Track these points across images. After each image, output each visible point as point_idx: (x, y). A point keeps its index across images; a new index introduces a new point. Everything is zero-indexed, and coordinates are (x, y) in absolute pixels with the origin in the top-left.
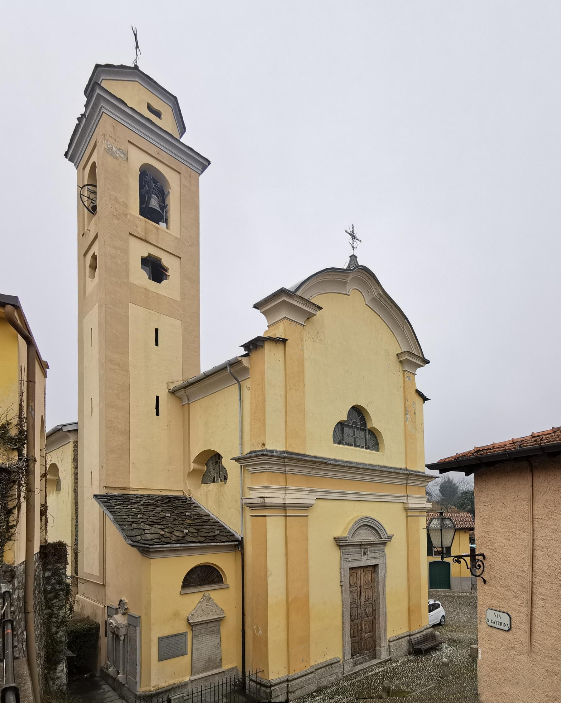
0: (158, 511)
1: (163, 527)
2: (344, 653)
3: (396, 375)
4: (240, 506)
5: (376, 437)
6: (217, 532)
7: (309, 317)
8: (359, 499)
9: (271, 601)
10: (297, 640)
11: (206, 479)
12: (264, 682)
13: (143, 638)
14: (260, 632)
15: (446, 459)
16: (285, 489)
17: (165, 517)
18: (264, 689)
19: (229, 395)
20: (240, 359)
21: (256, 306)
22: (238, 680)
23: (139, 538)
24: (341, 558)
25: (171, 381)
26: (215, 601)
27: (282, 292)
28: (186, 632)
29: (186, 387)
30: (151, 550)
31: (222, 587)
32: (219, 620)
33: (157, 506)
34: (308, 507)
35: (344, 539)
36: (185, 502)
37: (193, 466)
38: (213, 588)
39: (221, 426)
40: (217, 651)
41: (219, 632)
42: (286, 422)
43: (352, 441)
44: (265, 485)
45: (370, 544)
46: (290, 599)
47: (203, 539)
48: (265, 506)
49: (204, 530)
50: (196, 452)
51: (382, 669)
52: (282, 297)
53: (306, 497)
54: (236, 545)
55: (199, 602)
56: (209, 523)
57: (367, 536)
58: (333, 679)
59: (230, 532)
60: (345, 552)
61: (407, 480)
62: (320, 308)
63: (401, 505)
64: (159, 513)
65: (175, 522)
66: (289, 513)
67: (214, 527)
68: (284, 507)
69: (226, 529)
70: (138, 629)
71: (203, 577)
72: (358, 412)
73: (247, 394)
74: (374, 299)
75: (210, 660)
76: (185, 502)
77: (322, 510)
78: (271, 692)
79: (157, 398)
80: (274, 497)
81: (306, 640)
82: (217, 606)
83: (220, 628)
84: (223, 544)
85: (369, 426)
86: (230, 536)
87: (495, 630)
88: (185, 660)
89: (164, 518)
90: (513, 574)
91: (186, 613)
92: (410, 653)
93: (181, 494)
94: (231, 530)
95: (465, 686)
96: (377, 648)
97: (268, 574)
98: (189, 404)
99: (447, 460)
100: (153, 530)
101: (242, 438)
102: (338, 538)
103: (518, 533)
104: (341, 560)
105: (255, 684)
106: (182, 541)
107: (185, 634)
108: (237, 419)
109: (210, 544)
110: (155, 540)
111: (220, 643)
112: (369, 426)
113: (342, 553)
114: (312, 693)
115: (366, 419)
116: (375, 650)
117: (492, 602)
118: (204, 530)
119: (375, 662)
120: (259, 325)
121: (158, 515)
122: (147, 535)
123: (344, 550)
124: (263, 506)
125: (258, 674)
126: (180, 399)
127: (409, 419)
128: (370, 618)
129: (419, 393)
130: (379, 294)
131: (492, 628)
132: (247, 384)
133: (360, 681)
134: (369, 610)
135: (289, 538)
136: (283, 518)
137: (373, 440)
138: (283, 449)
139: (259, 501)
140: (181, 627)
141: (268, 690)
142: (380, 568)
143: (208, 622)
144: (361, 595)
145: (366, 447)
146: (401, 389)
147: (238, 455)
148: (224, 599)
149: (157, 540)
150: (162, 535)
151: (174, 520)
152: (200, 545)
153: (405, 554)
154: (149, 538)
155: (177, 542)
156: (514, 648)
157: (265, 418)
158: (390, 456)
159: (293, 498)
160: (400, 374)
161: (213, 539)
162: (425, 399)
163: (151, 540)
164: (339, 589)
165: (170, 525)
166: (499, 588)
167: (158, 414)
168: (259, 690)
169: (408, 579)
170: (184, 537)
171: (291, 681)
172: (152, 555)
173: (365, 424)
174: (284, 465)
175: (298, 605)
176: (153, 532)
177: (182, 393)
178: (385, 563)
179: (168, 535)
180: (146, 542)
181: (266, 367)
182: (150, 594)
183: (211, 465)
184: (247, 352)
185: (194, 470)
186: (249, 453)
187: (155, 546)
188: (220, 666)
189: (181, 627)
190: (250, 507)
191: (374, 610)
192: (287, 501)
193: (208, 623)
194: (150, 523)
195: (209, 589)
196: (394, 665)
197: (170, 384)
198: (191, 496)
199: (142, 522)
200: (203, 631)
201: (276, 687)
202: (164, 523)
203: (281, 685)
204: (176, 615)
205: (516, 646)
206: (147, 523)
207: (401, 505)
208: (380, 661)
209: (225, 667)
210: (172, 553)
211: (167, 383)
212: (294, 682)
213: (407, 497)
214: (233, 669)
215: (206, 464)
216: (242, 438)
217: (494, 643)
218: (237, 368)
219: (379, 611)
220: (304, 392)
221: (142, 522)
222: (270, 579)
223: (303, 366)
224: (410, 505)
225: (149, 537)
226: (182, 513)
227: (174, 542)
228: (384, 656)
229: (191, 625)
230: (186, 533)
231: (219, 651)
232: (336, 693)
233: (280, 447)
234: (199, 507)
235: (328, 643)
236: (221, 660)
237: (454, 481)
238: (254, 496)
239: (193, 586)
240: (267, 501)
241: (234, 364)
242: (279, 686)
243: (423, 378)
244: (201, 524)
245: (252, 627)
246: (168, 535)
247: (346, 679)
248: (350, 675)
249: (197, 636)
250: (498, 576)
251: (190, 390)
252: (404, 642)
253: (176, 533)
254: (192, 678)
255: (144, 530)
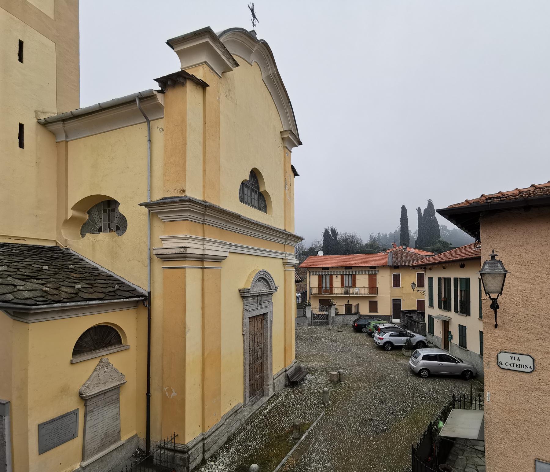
0: (30, 263)
1: (42, 282)
2: (245, 397)
3: (280, 151)
4: (145, 256)
5: (265, 201)
6: (116, 287)
7: (226, 69)
8: (257, 254)
9: (189, 359)
10: (209, 393)
11: (87, 228)
12: (179, 447)
13: (14, 429)
14: (174, 394)
15: (457, 204)
16: (204, 240)
17: (41, 270)
18: (180, 455)
19: (134, 135)
20: (155, 93)
21: (171, 43)
22: (140, 450)
23: (10, 297)
24: (243, 308)
25: (41, 109)
26: (114, 366)
27: (207, 32)
28: (78, 410)
29: (64, 120)
30: (33, 312)
31: (122, 349)
32: (117, 388)
33: (25, 257)
34: (222, 260)
35: (248, 291)
36: (62, 253)
37: (71, 213)
38: (111, 351)
39: (118, 167)
40: (115, 423)
41: (118, 400)
42: (204, 171)
43: (249, 202)
44: (185, 234)
45: (264, 295)
46: (206, 354)
47: (102, 296)
48: (185, 257)
49: (99, 285)
50: (77, 195)
51: (273, 405)
52: (205, 38)
53: (219, 249)
54: (137, 302)
55: (95, 370)
56: (101, 277)
57: (262, 288)
58: (237, 426)
59: (130, 286)
60: (247, 303)
61: (286, 239)
62: (237, 65)
63: (280, 261)
64: (30, 265)
65: (57, 276)
66: (206, 265)
67: (110, 281)
68: (202, 259)
69: (123, 283)
70: (6, 419)
71: (101, 339)
72: (255, 174)
73: (159, 137)
74: (268, 77)
75: (106, 435)
76: (62, 253)
77: (233, 262)
78: (189, 457)
79: (21, 126)
80: (195, 248)
81: (217, 393)
82: (116, 371)
83: (119, 395)
84: (128, 300)
85: (261, 190)
86: (132, 292)
87: (510, 373)
88: (76, 444)
89: (40, 271)
90: (538, 317)
91: (77, 386)
92: (286, 386)
93: (53, 245)
94: (131, 285)
95: (346, 409)
96: (265, 387)
97: (187, 330)
98: (67, 142)
99: (459, 206)
100: (29, 286)
101: (150, 183)
102: (244, 290)
103: (546, 277)
104: (243, 311)
105: (166, 452)
106: (77, 299)
107: (75, 413)
108: (144, 163)
109: (113, 301)
110: (37, 299)
111: (118, 414)
112: (261, 190)
113: (244, 304)
114: (224, 444)
115: (259, 182)
116: (263, 389)
117: (506, 345)
118: (99, 285)
119: (265, 399)
120: (173, 64)
121: (30, 267)
122: (23, 293)
123: (247, 301)
124: (183, 257)
125: (173, 441)
126: (54, 134)
127: (287, 189)
128: (260, 361)
129: (293, 168)
130: (273, 73)
131: (505, 371)
132: (158, 125)
133: (261, 422)
134: (260, 354)
135: (206, 291)
136: (200, 270)
137: (262, 201)
138: (161, 197)
139: (178, 251)
140: (71, 404)
141: (186, 456)
142: (269, 315)
143: (104, 393)
144: (255, 342)
145: (258, 208)
146: (282, 162)
147: (146, 200)
148: (124, 363)
149: (41, 299)
150: (46, 292)
151: (56, 274)
152: (100, 302)
153: (283, 302)
154: (27, 296)
155: (70, 300)
156: (539, 390)
157: (185, 162)
158: (273, 219)
159: (212, 250)
160: (282, 149)
161: (113, 295)
162: (296, 174)
163: (30, 298)
164: (241, 338)
165: (52, 279)
166: (516, 332)
167: (21, 145)
168: (173, 458)
169: (285, 324)
170: (76, 294)
171: (206, 439)
172: (31, 319)
173: (258, 187)
174: (204, 215)
175: (210, 358)
176: (30, 288)
177: (59, 126)
178: (272, 311)
179: (55, 292)
180: (25, 302)
181: (188, 108)
182: (26, 370)
183: (102, 213)
184: (160, 89)
185: (73, 218)
186: (162, 199)
187: (39, 307)
188: (119, 439)
189: (71, 404)
190: (162, 258)
191: (263, 354)
192: (207, 252)
193: (105, 393)
194: (22, 277)
195: (105, 353)
196: (280, 399)
197: (39, 113)
198: (68, 247)
199: (9, 275)
200: (100, 402)
201: (193, 449)
202: (43, 277)
203: (197, 446)
204: (64, 390)
205: (543, 387)
206: (17, 276)
207: (281, 261)
208: (268, 398)
209: (124, 439)
210: (60, 315)
211: (36, 112)
212: (209, 439)
213: (286, 254)
214: (132, 438)
215: (89, 213)
216: (150, 183)
217: (509, 385)
218: (148, 104)
219: (268, 354)
220: (219, 144)
221: (9, 275)
222: (188, 336)
223: (219, 117)
224: (289, 261)
225: (27, 295)
226: (62, 265)
227: (65, 300)
228: (271, 393)
229: (83, 399)
230: (78, 289)
231: (118, 422)
232: (247, 439)
233: (198, 197)
234: (82, 259)
235: (233, 391)
236: (119, 432)
237: (388, 234)
238: (172, 247)
239: (86, 352)
240: (189, 251)
241: (146, 98)
242: (195, 447)
243: (297, 156)
244: (92, 278)
245: (162, 388)
246: (55, 292)
247: (248, 422)
248: (249, 417)
249: (92, 411)
250: (515, 320)
251: (70, 125)
252: (282, 377)
253: (64, 289)
254: (85, 464)
255: (15, 286)
